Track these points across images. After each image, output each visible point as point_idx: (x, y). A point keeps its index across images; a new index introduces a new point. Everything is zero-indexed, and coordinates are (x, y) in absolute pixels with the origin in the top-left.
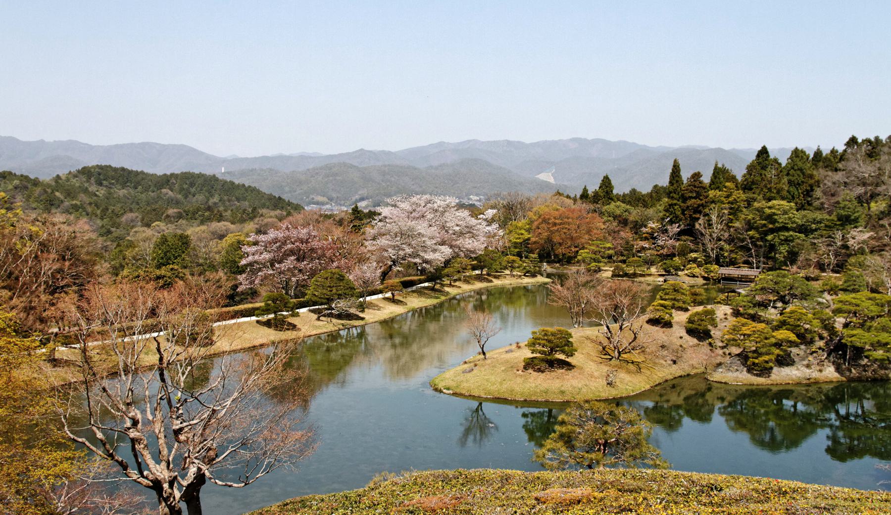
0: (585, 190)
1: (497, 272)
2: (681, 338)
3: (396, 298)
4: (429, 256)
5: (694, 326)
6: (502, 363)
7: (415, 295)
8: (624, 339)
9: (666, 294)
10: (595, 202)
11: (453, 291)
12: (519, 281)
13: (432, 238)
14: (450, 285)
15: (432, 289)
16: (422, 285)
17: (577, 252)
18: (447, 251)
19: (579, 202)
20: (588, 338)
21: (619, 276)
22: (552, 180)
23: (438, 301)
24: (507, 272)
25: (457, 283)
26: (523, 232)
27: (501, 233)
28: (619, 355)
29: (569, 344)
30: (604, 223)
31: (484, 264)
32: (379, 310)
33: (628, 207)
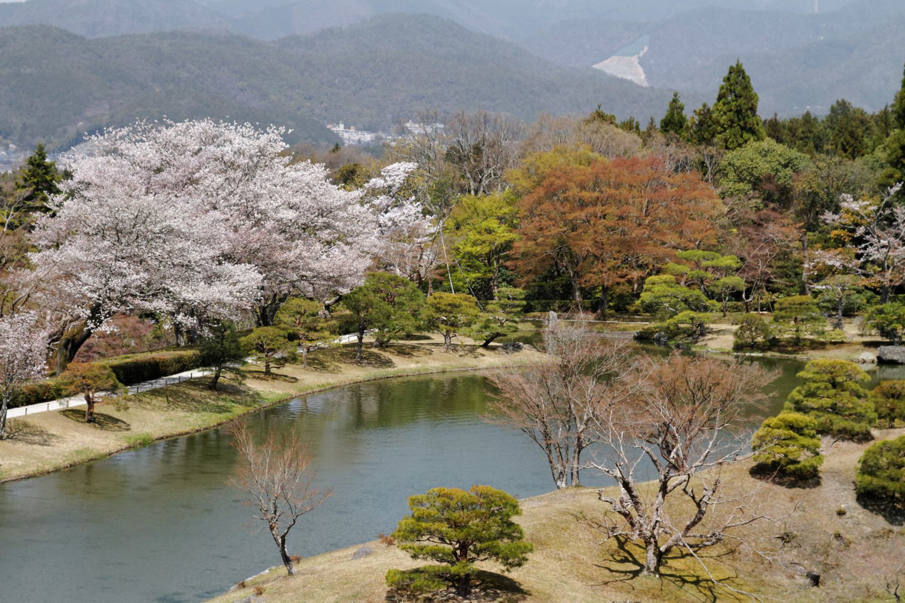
0: (676, 106)
1: (409, 337)
2: (841, 513)
3: (97, 409)
4: (196, 293)
5: (876, 482)
6: (332, 587)
7: (160, 401)
8: (666, 517)
9: (811, 394)
10: (702, 140)
11: (269, 391)
12: (470, 361)
13: (209, 241)
14: (268, 374)
15: (213, 385)
16: (186, 374)
17: (642, 280)
18: (248, 277)
19: (659, 138)
20: (580, 517)
21: (754, 346)
22: (638, 76)
23: (223, 417)
24: (438, 338)
25: (288, 370)
26: (493, 224)
27: (428, 226)
28: (659, 563)
29: (509, 530)
30: (723, 196)
31: (367, 314)
32: (44, 443)
33: (794, 153)
